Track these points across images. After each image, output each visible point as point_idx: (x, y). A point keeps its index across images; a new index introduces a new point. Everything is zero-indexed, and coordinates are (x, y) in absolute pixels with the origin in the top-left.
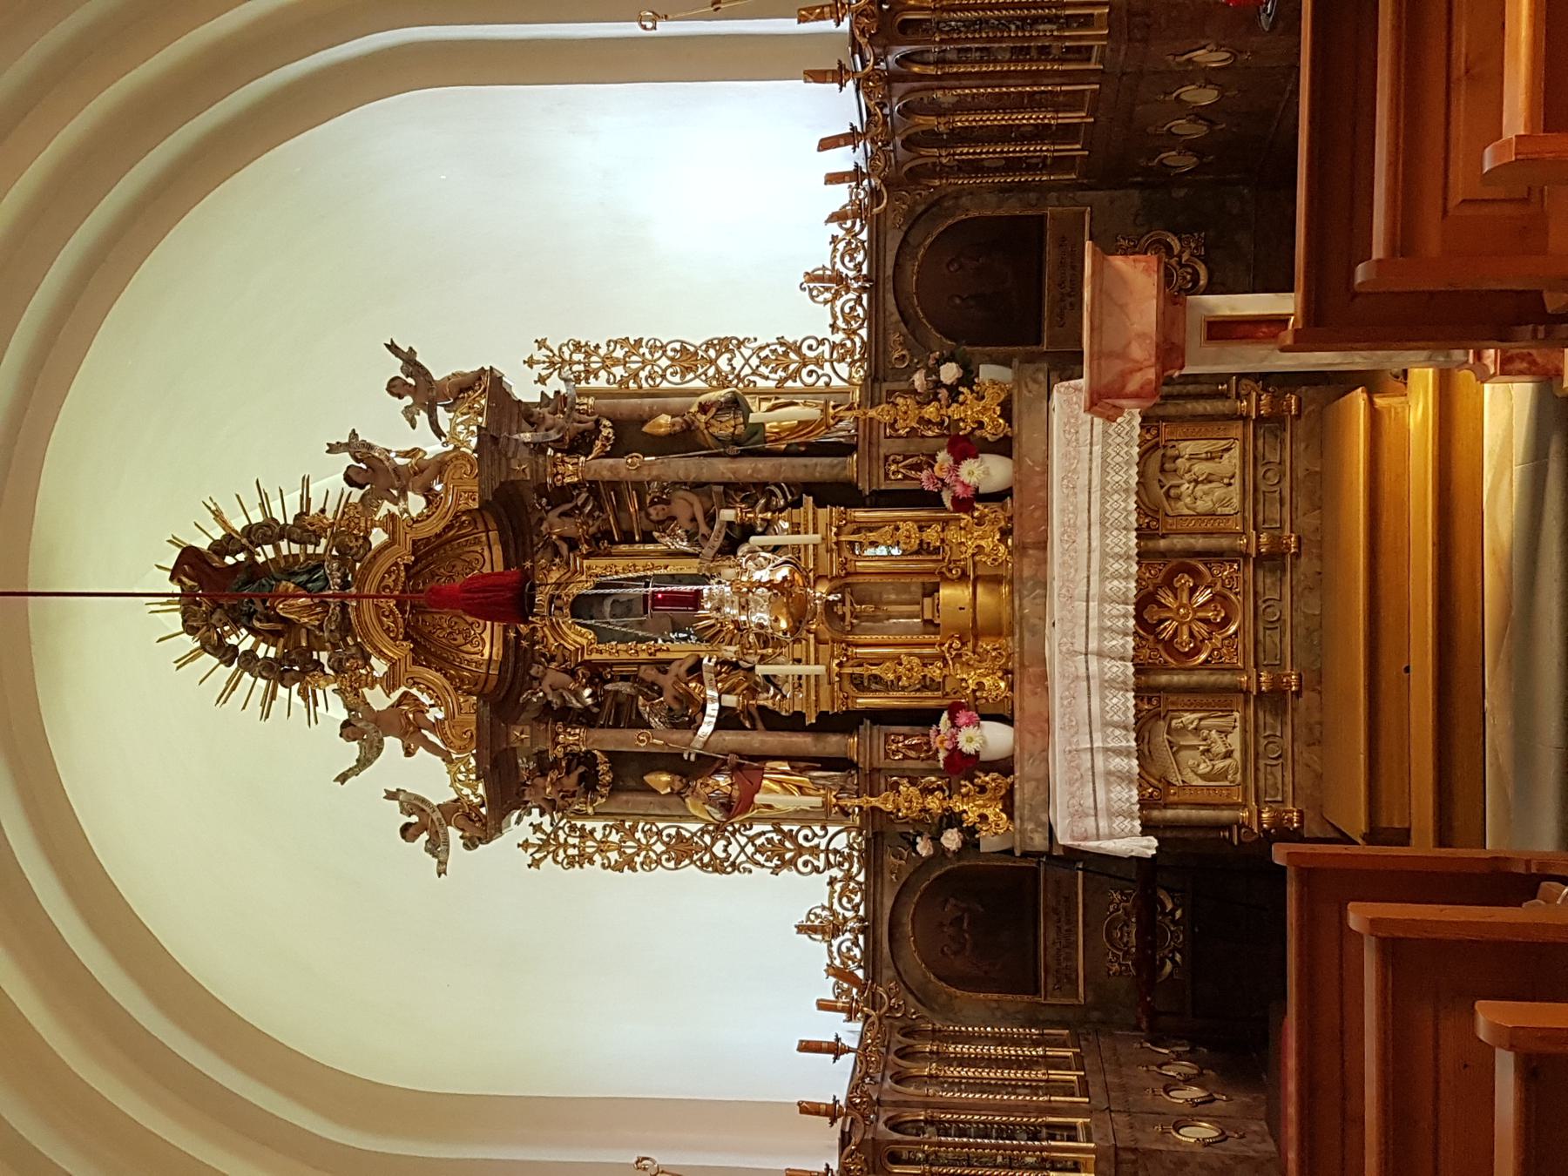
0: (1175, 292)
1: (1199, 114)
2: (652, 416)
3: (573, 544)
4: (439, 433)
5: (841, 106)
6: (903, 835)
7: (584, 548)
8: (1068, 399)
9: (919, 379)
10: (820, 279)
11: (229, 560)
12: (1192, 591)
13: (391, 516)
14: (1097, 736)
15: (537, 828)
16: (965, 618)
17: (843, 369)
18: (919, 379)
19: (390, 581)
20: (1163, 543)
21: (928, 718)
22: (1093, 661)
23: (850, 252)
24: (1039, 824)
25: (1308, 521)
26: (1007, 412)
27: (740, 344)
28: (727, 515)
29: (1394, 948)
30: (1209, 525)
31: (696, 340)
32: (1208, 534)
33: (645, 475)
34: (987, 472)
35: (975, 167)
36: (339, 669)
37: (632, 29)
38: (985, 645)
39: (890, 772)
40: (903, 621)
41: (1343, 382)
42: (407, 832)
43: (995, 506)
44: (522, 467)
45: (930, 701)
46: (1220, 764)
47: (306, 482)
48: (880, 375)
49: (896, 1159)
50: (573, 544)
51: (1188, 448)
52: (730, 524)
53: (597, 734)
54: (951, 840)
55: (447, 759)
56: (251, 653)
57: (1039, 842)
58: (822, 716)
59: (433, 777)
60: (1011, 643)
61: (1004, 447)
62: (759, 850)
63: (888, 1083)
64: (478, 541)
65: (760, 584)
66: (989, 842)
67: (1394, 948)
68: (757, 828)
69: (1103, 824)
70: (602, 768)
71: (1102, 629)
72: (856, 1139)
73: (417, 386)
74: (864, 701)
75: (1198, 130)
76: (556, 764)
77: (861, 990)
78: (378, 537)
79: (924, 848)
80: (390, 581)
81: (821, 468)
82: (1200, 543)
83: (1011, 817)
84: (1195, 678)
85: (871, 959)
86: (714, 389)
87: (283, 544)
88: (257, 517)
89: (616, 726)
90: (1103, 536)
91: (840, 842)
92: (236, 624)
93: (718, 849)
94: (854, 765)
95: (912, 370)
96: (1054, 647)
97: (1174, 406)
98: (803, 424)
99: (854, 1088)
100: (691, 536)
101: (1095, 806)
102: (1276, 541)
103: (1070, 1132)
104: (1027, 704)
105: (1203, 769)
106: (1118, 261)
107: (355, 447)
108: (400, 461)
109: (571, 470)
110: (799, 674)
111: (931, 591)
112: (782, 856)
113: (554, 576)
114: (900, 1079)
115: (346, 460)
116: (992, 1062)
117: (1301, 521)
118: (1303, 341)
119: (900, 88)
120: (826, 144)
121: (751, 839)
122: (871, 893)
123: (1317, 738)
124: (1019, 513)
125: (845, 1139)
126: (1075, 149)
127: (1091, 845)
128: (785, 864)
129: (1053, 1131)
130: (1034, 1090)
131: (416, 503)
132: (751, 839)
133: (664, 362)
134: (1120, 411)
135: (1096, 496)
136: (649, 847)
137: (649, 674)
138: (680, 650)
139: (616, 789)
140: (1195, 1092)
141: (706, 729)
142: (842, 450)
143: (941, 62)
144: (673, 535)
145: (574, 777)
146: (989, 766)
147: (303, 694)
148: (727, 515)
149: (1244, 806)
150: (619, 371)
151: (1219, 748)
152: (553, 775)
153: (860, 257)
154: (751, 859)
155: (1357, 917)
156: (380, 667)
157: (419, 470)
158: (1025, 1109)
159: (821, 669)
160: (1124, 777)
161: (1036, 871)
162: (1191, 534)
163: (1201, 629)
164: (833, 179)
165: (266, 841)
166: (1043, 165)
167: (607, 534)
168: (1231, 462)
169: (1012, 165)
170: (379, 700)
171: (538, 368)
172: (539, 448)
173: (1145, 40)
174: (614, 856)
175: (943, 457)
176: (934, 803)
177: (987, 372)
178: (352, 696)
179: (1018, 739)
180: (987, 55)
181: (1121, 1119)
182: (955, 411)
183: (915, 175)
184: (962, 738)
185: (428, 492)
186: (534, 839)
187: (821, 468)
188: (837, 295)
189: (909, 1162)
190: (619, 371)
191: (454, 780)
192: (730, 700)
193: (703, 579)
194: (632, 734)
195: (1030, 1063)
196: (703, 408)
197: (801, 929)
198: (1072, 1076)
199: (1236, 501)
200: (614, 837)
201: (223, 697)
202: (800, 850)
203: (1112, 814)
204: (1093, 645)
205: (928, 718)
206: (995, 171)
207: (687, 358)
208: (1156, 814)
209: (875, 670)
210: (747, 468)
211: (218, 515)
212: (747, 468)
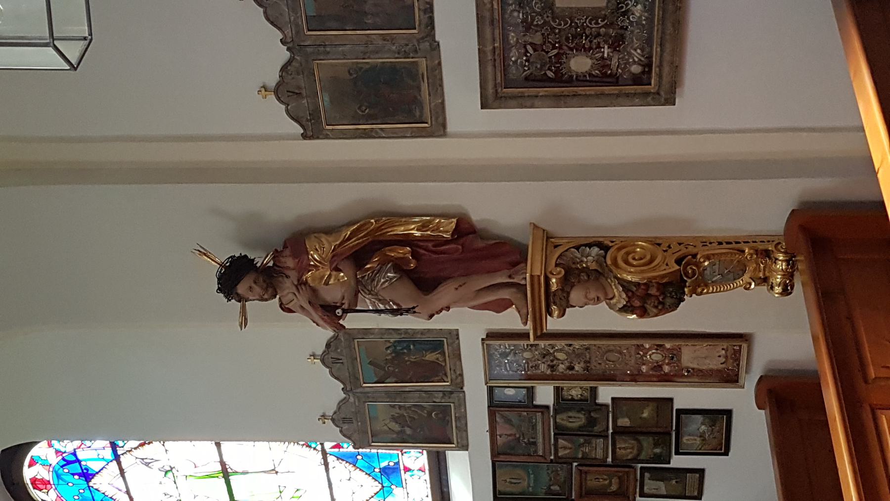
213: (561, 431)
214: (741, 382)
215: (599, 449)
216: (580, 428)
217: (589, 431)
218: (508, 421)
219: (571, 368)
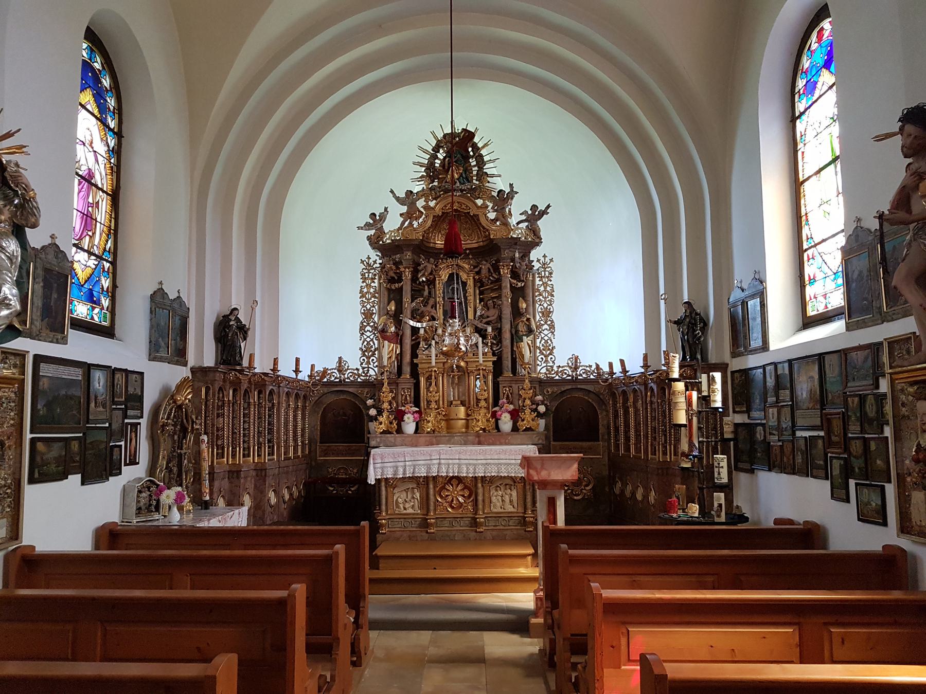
0: (562, 485)
1: (633, 494)
2: (526, 301)
3: (478, 273)
4: (518, 224)
5: (635, 368)
6: (374, 395)
7: (477, 277)
8: (531, 450)
9: (539, 398)
10: (576, 361)
11: (470, 149)
12: (463, 496)
13: (487, 207)
14: (410, 463)
15: (375, 262)
16: (453, 416)
17: (544, 370)
18: (539, 398)
19: (463, 207)
20: (480, 485)
21: (417, 403)
22: (437, 461)
23: (586, 372)
24: (379, 443)
25: (489, 535)
26: (527, 429)
27: (553, 333)
28: (490, 329)
29: (329, 560)
30: (487, 501)
31: (554, 317)
32: (483, 501)
33: (504, 299)
34: (506, 423)
35: (616, 416)
36: (431, 189)
37: (662, 291)
38: (443, 423)
39: (397, 389)
40: (452, 394)
41: (535, 548)
42: (373, 215)
43: (494, 426)
44: (506, 254)
45: (423, 404)
46: (401, 506)
47: (500, 176)
48: (541, 384)
49: (260, 393)
50: (478, 273)
51: (514, 493)
52: (486, 330)
53: (409, 283)
54: (373, 412)
55: (399, 229)
56: (437, 158)
57: (373, 443)
58: (417, 365)
59: (392, 224)
60: (444, 433)
61: (515, 429)
62: (368, 343)
63: (286, 390)
64: (479, 238)
65: (459, 340)
66: (372, 425)
67: (329, 560)
68: (376, 342)
69: (378, 465)
70: (397, 285)
71: (449, 465)
72: (266, 378)
73: (535, 215)
74: (422, 380)
75: (628, 493)
76: (398, 268)
77: (319, 380)
78: (479, 202)
79: (370, 402)
80: (463, 207)
81: (507, 363)
82: (480, 498)
83: (381, 433)
84: (432, 497)
85: (330, 384)
86: (536, 323)
87: (476, 168)
88: (486, 159)
89: (412, 290)
90: (482, 464)
91: (371, 372)
92: (447, 152)
93: (368, 328)
94: (399, 377)
95: (542, 394)
96: (443, 448)
97: (526, 486)
98: (523, 356)
99: (284, 378)
100: (481, 316)
101: (384, 463)
102: (481, 524)
103: (271, 454)
104: (422, 438)
105: (400, 500)
106: (576, 466)
107: (512, 193)
108: (507, 210)
109: (505, 272)
110: (431, 357)
111: (463, 404)
112: (366, 351)
113: (467, 266)
114: (288, 394)
115: (507, 190)
116: (295, 427)
117: (488, 532)
118: (545, 528)
119: (643, 388)
120: (622, 362)
121: (372, 340)
122: (354, 383)
123: (412, 539)
124: (491, 435)
125: (266, 374)
126: (622, 451)
127: (371, 461)
128: (364, 352)
129: (271, 448)
130: (286, 441)
131: (492, 215)
132: (372, 340)
133: (545, 305)
134: (523, 468)
135: (496, 461)
136: (369, 303)
137: (431, 302)
138: (440, 313)
139: (389, 290)
140: (287, 497)
141: (412, 323)
142: (514, 370)
143: (652, 402)
144: (482, 309)
145: (393, 275)
146: (399, 425)
147: (422, 177)
148: (490, 329)
149: (387, 514)
150: (542, 289)
151: (407, 505)
152: (394, 267)
153: (584, 376)
154: (365, 340)
155: (339, 547)
156: (432, 204)
157: (504, 216)
158: (279, 438)
159: (434, 364)
160: (396, 473)
161: (363, 442)
162: (484, 495)
163: (450, 499)
164: (611, 365)
165: (371, 162)
166: (617, 440)
167: (482, 285)
168: (509, 508)
169: (617, 429)
170: (420, 204)
171: (542, 259)
172: (513, 260)
173: (658, 474)
174: (365, 290)
175: (511, 407)
176: (386, 405)
177: (542, 422)
178: (421, 194)
179: (409, 435)
180: (653, 418)
181: (276, 471)
182: (528, 411)
183: (613, 395)
184: (409, 415)
185: (496, 220)
186: (371, 261)
187: (507, 363)
188: (571, 368)
189: (259, 397)
190: (542, 289)
191: (392, 232)
192: (422, 331)
193: (464, 319)
194: (409, 296)
195: (295, 440)
196: (528, 320)
197: (340, 358)
198: (291, 454)
199: (495, 510)
200: (372, 290)
201: (421, 148)
202: (368, 358)
203: (382, 468)
204: (443, 461)
205: (417, 403)
206: (615, 423)
207: (547, 313)
208: (383, 484)
209: (433, 384)
210: (507, 336)
211: (485, 145)
212: (507, 336)
213: (862, 399)
214: (902, 535)
215: (854, 430)
216: (866, 413)
217: (864, 420)
218: (866, 358)
219: (903, 405)
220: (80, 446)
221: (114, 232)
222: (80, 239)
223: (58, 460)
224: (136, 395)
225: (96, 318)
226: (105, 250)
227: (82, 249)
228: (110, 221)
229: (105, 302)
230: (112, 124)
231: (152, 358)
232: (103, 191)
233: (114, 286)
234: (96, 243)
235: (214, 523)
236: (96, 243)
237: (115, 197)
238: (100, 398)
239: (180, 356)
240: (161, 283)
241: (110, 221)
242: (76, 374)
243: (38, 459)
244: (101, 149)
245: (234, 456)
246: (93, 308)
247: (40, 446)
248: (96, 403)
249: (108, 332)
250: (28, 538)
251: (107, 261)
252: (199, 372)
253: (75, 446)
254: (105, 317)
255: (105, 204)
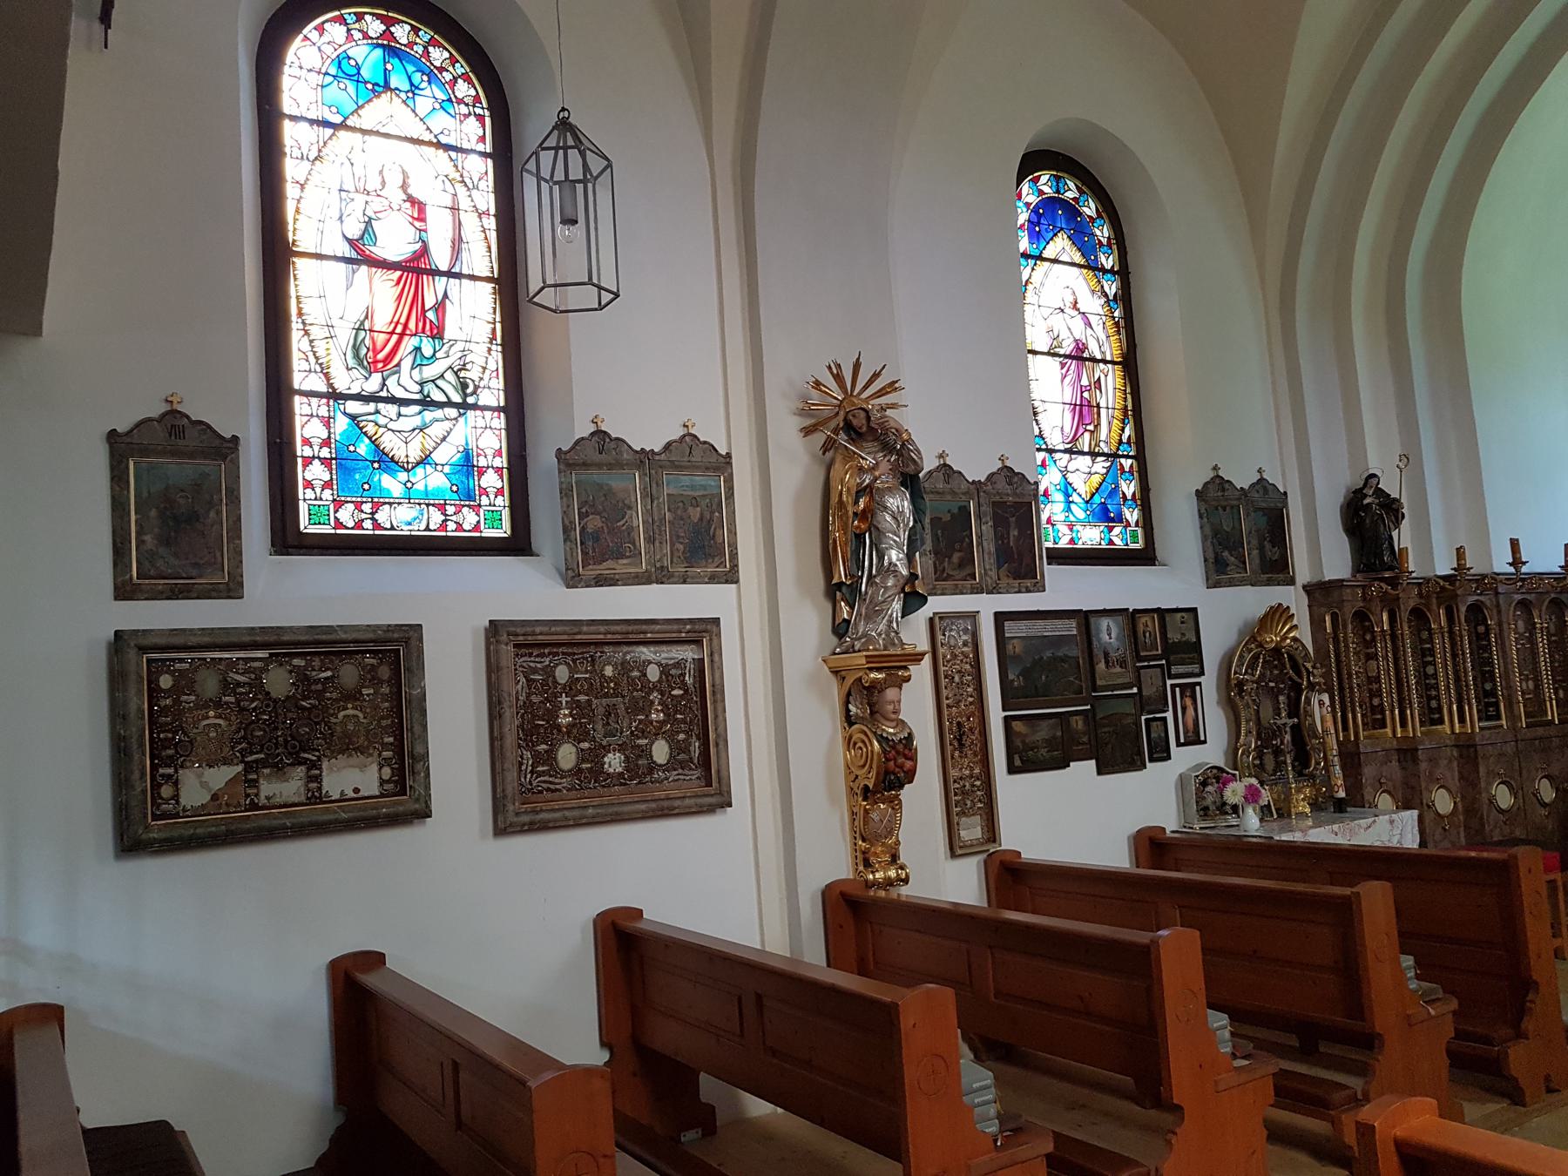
220: (1086, 722)
221: (1135, 411)
222: (1075, 439)
223: (1050, 743)
224: (1187, 643)
225: (1117, 541)
226: (1120, 442)
227: (1082, 453)
228: (1125, 399)
229: (1132, 515)
230: (1108, 262)
231: (1212, 584)
232: (1105, 362)
233: (1144, 488)
234: (1103, 437)
235: (1297, 837)
236: (1103, 437)
237: (1129, 364)
238: (1113, 655)
239: (1277, 569)
240: (1215, 468)
241: (1125, 399)
242: (1070, 628)
243: (1018, 743)
244: (1093, 305)
245: (1404, 724)
246: (1111, 529)
247: (1018, 726)
248: (1107, 662)
249: (1145, 557)
250: (1008, 841)
251: (1127, 457)
252: (1319, 592)
253: (1078, 724)
254: (1134, 536)
255: (1112, 380)
